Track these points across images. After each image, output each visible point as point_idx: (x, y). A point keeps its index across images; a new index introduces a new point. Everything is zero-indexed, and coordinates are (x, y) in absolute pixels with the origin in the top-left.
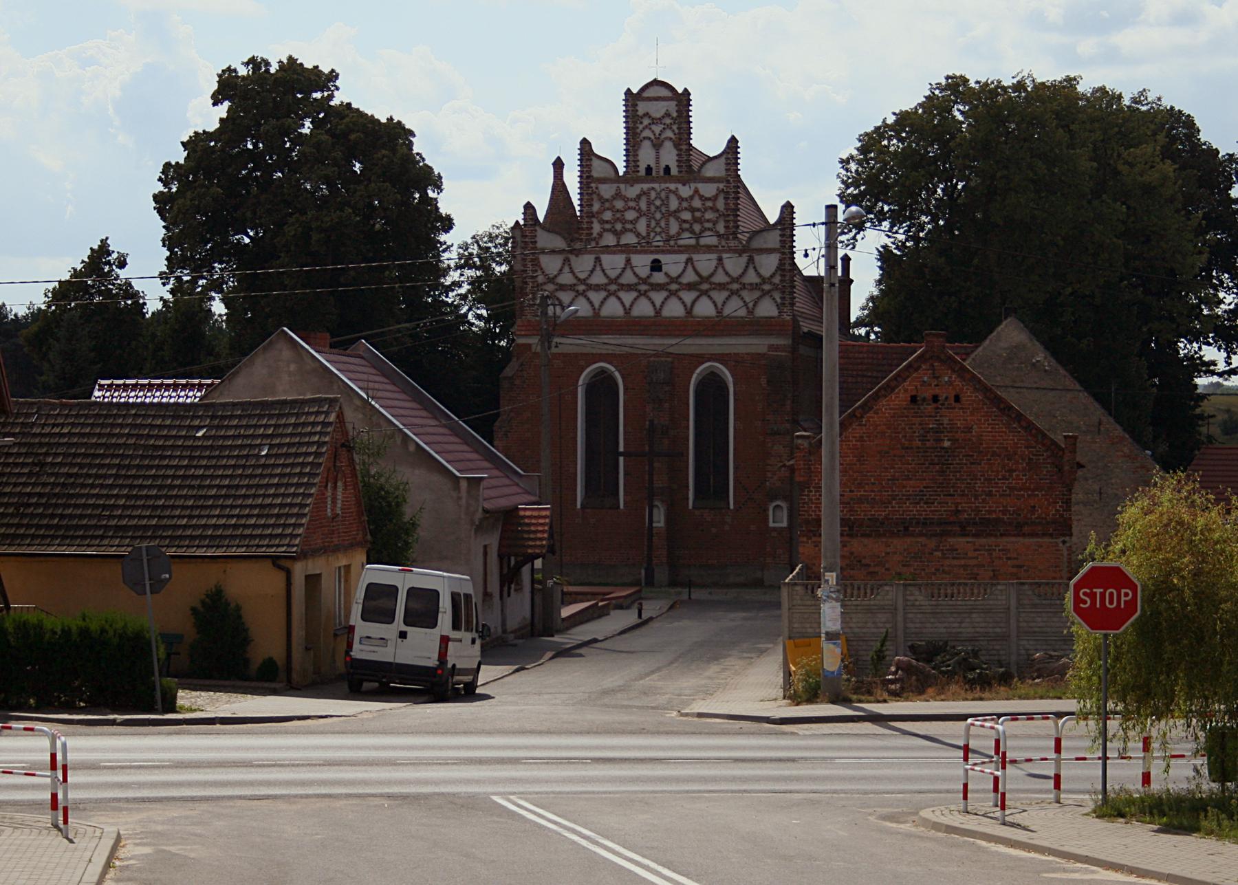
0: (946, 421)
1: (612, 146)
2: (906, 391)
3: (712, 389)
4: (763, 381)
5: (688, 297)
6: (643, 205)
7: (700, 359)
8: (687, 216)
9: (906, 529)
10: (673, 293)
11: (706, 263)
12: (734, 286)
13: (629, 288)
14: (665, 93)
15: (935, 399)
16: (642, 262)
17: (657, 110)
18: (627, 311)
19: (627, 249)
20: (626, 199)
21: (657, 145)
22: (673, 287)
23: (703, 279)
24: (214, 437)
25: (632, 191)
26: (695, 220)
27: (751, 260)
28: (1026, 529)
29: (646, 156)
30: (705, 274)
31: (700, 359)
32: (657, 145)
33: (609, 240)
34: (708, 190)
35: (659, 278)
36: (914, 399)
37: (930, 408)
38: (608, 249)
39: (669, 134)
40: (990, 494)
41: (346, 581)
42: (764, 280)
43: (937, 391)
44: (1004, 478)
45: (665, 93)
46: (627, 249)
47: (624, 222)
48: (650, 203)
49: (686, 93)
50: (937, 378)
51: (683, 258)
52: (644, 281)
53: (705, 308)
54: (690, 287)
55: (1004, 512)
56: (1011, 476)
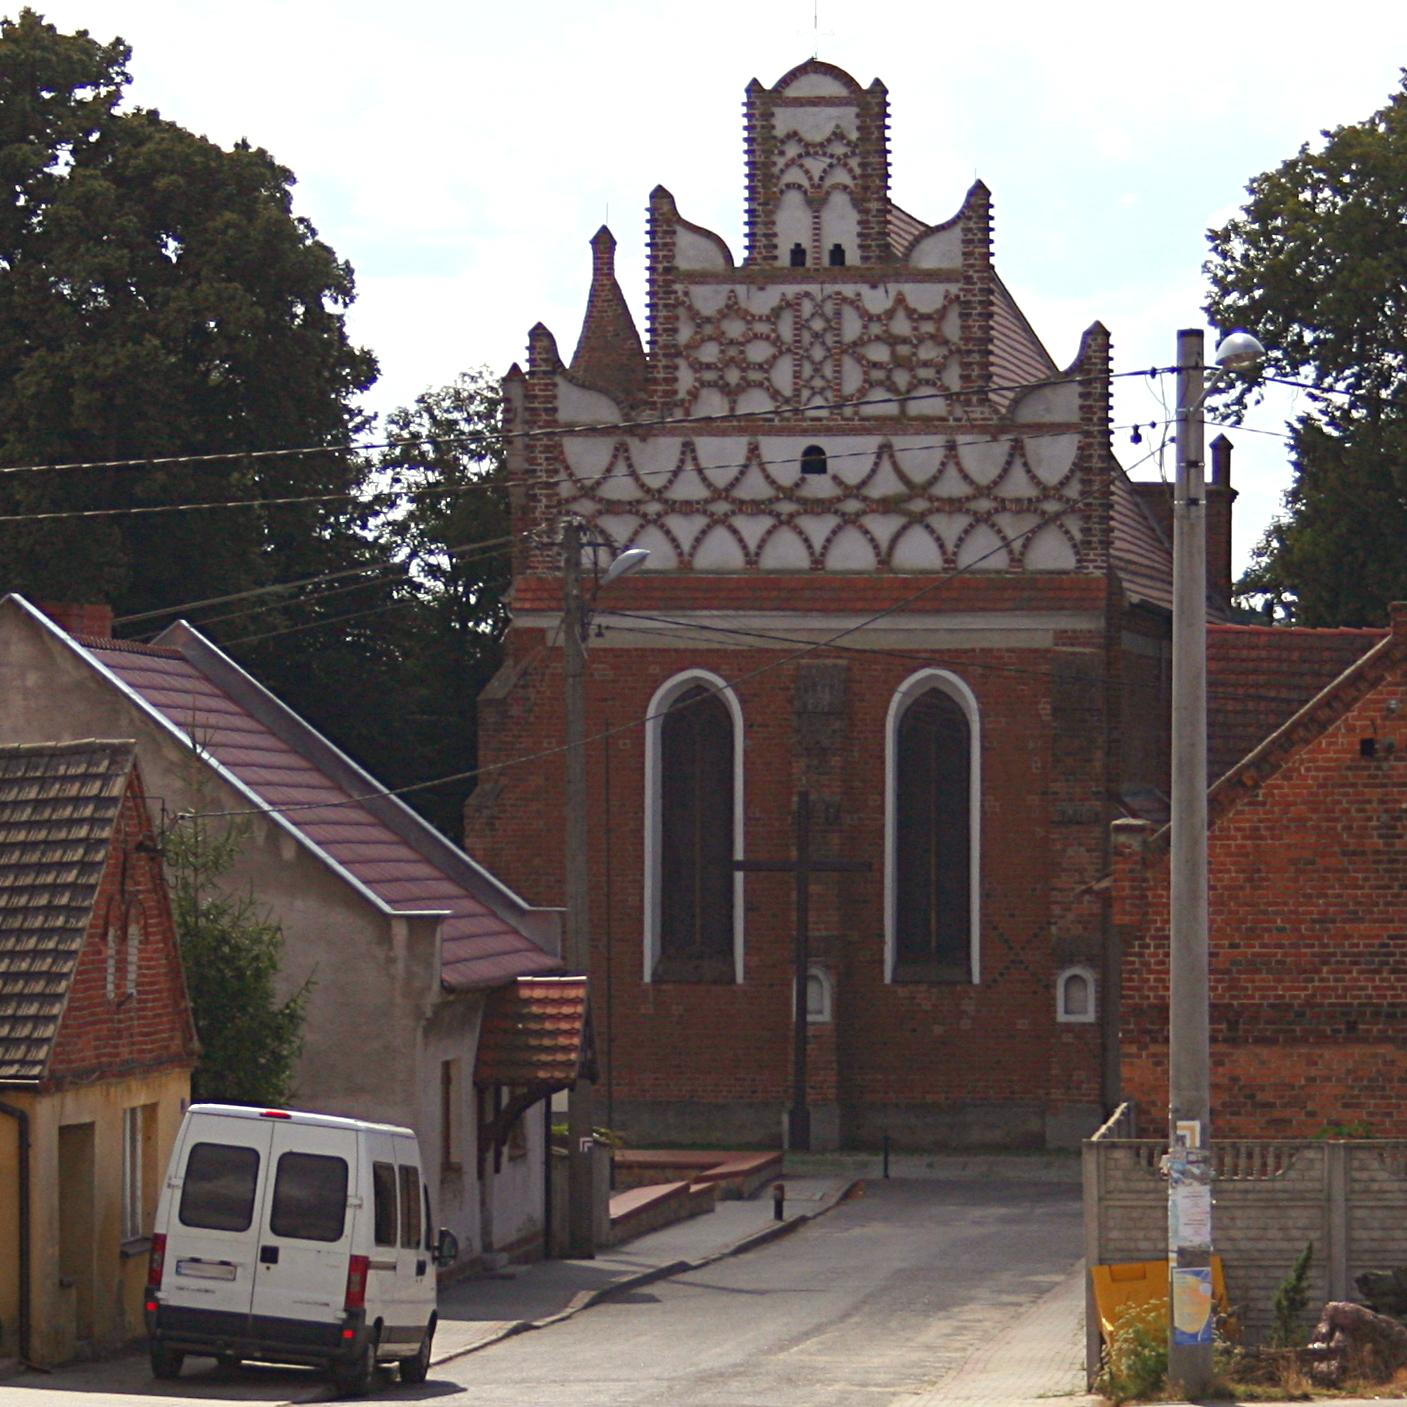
2: (1351, 729)
3: (934, 717)
4: (1045, 708)
5: (883, 527)
6: (786, 330)
7: (909, 660)
8: (879, 353)
10: (850, 520)
11: (920, 455)
12: (982, 505)
13: (756, 508)
14: (833, 88)
16: (783, 454)
17: (816, 124)
19: (751, 426)
20: (748, 318)
21: (816, 201)
22: (850, 507)
23: (915, 490)
25: (762, 301)
26: (899, 362)
27: (1018, 448)
29: (793, 224)
30: (919, 477)
31: (909, 660)
32: (816, 201)
33: (713, 405)
34: (926, 297)
35: (819, 486)
36: (1368, 747)
39: (841, 177)
41: (148, 1139)
42: (1046, 492)
45: (833, 88)
46: (751, 426)
47: (745, 366)
48: (800, 326)
51: (872, 443)
52: (789, 493)
53: (918, 553)
54: (887, 506)
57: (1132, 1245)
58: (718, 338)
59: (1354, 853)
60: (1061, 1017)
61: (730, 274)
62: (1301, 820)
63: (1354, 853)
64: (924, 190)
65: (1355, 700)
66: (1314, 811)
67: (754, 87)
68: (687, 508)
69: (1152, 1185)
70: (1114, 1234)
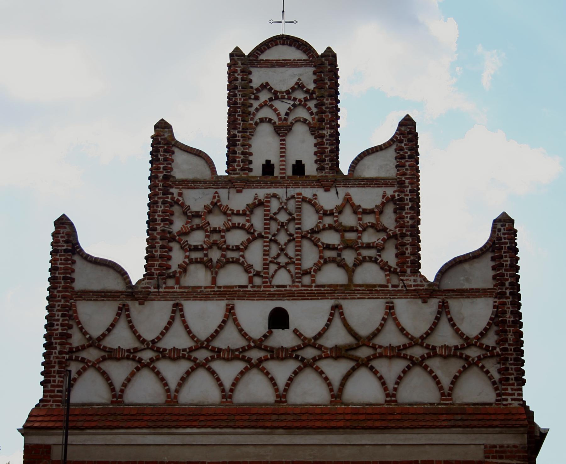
1: (206, 129)
5: (335, 370)
8: (331, 238)
10: (307, 364)
12: (416, 353)
13: (232, 355)
16: (254, 316)
17: (283, 79)
19: (231, 294)
20: (226, 212)
21: (282, 130)
22: (308, 354)
23: (361, 341)
25: (239, 200)
26: (348, 245)
29: (264, 147)
30: (364, 331)
32: (282, 130)
33: (198, 277)
34: (368, 198)
35: (283, 339)
38: (197, 294)
39: (302, 113)
42: (468, 342)
48: (270, 218)
51: (326, 305)
52: (259, 344)
53: (364, 390)
54: (339, 353)
61: (216, 182)
64: (361, 130)
67: (236, 54)
68: (175, 355)
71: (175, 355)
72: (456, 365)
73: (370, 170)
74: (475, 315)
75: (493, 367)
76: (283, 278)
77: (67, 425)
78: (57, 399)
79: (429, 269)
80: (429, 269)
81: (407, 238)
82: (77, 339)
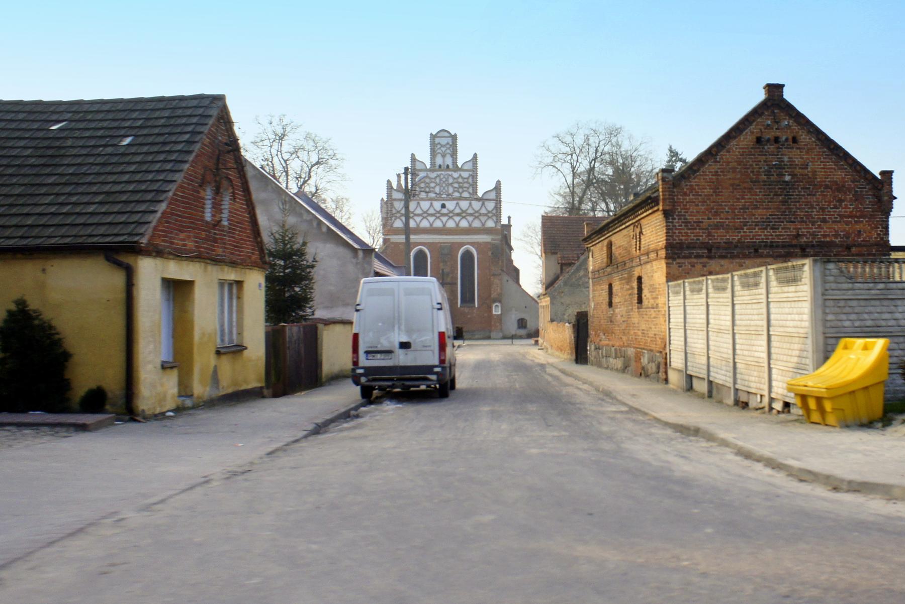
0: (786, 159)
1: (424, 157)
2: (752, 133)
3: (468, 256)
4: (490, 253)
5: (457, 219)
6: (438, 180)
7: (462, 244)
8: (456, 185)
9: (756, 251)
10: (450, 218)
11: (464, 205)
12: (476, 215)
13: (432, 215)
14: (447, 134)
15: (777, 140)
16: (437, 205)
17: (444, 141)
18: (431, 225)
19: (431, 199)
20: (430, 178)
21: (444, 156)
22: (451, 215)
23: (463, 212)
24: (72, 129)
25: (433, 175)
26: (460, 187)
27: (483, 204)
28: (854, 250)
29: (439, 160)
30: (464, 209)
31: (462, 244)
32: (444, 156)
33: (423, 195)
34: (465, 175)
35: (444, 211)
36: (759, 140)
37: (772, 148)
38: (423, 199)
39: (448, 151)
40: (824, 221)
41: (239, 298)
42: (489, 212)
43: (778, 134)
44: (835, 207)
45: (447, 134)
46: (431, 199)
47: (429, 188)
48: (441, 180)
49: (456, 135)
50: (777, 123)
51: (455, 202)
52: (439, 212)
53: (464, 224)
54: (458, 215)
55: (836, 236)
56: (841, 205)
57: (839, 324)
58: (424, 182)
59: (755, 182)
60: (494, 313)
61: (427, 170)
62: (734, 169)
63: (755, 182)
64: (463, 157)
65: (754, 121)
66: (739, 165)
67: (431, 134)
68: (418, 215)
69: (850, 285)
70: (830, 317)
71: (418, 215)
72: (486, 218)
73: (465, 167)
74: (491, 206)
75: (494, 218)
76: (444, 196)
77: (407, 224)
78: (235, 320)
79: (480, 194)
80: (480, 194)
81: (474, 185)
82: (394, 211)
